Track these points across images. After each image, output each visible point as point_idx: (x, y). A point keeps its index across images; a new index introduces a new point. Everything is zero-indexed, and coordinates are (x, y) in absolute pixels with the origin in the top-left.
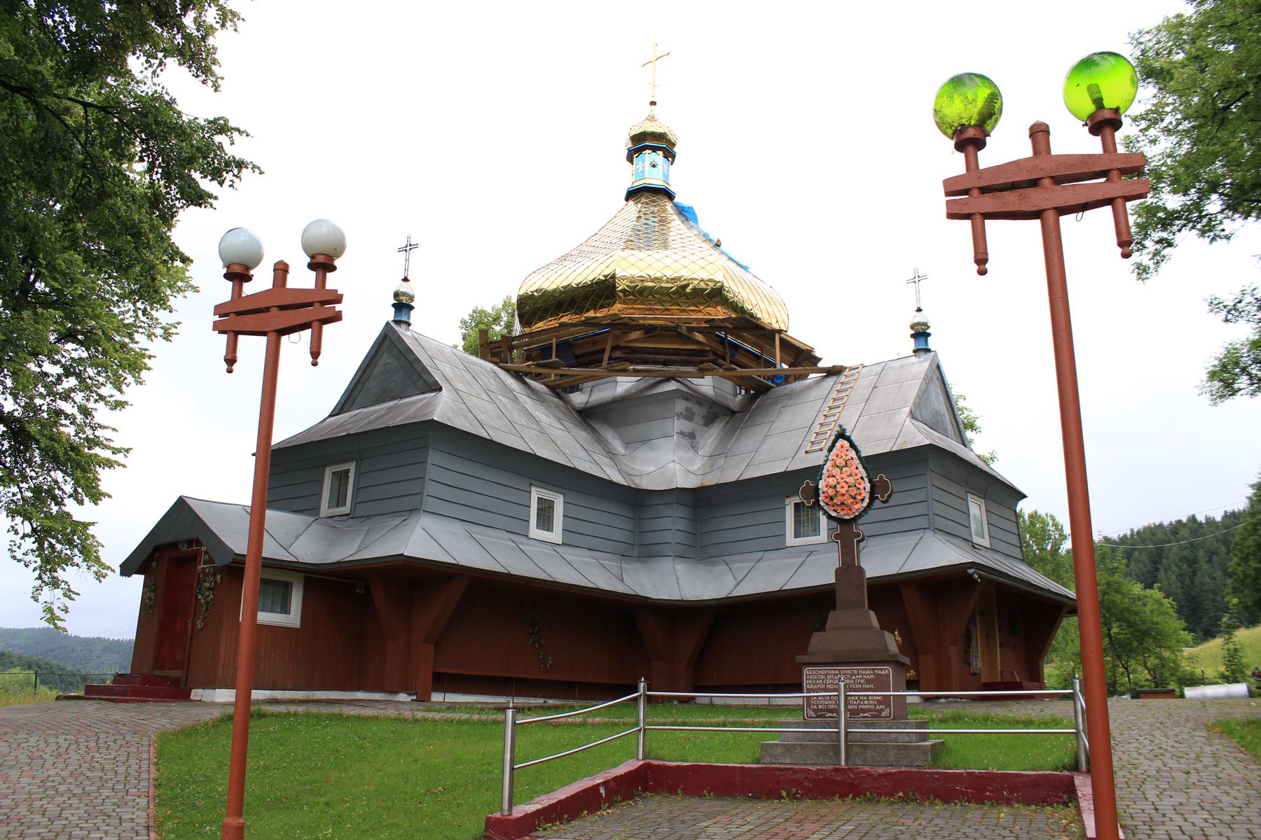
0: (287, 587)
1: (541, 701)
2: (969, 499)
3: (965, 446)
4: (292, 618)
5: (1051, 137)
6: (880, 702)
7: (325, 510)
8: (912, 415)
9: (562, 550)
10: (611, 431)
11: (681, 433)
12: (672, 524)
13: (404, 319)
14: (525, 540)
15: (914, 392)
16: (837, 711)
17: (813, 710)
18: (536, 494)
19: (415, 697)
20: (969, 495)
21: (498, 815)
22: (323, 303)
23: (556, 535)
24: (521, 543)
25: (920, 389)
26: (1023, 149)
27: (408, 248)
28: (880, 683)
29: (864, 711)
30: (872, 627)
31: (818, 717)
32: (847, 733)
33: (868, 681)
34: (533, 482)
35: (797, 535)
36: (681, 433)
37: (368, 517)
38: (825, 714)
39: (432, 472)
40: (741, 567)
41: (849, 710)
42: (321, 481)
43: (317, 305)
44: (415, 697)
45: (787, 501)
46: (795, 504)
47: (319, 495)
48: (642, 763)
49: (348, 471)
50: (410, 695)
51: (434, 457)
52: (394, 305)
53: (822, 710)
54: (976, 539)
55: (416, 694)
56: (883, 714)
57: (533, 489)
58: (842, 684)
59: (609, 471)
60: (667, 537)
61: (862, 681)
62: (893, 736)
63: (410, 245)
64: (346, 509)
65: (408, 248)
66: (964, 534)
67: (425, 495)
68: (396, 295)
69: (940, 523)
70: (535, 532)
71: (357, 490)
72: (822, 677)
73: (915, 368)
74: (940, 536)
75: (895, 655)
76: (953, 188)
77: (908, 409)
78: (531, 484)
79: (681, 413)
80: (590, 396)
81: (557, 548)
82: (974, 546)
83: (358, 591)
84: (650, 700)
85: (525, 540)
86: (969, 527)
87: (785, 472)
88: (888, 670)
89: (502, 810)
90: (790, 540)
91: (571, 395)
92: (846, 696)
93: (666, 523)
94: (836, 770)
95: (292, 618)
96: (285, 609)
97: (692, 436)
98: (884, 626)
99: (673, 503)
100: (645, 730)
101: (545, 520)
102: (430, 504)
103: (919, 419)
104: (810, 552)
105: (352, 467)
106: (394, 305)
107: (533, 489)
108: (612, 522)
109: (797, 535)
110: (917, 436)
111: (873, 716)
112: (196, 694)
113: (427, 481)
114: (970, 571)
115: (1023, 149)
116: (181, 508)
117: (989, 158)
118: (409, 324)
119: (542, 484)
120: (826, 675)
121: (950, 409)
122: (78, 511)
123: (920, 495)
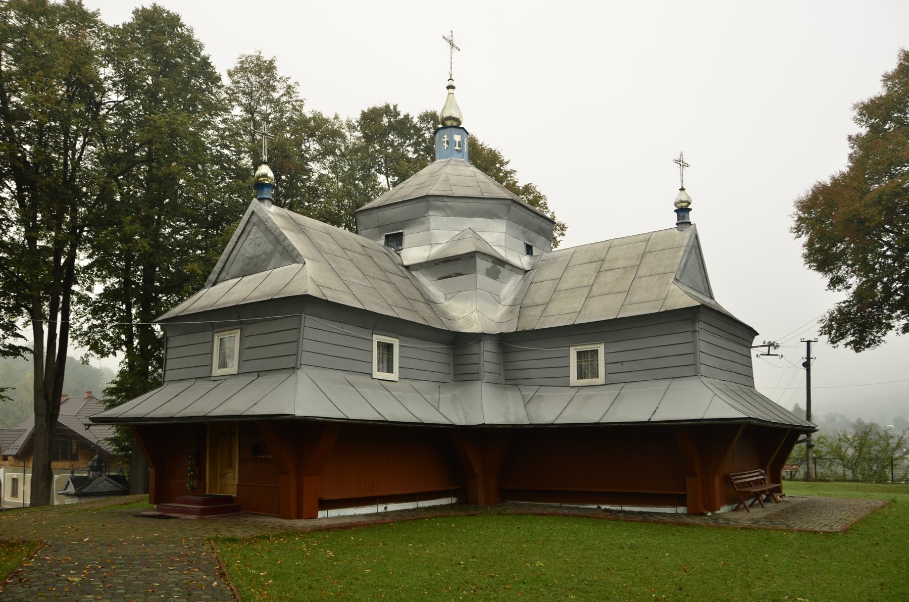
18: (377, 338)
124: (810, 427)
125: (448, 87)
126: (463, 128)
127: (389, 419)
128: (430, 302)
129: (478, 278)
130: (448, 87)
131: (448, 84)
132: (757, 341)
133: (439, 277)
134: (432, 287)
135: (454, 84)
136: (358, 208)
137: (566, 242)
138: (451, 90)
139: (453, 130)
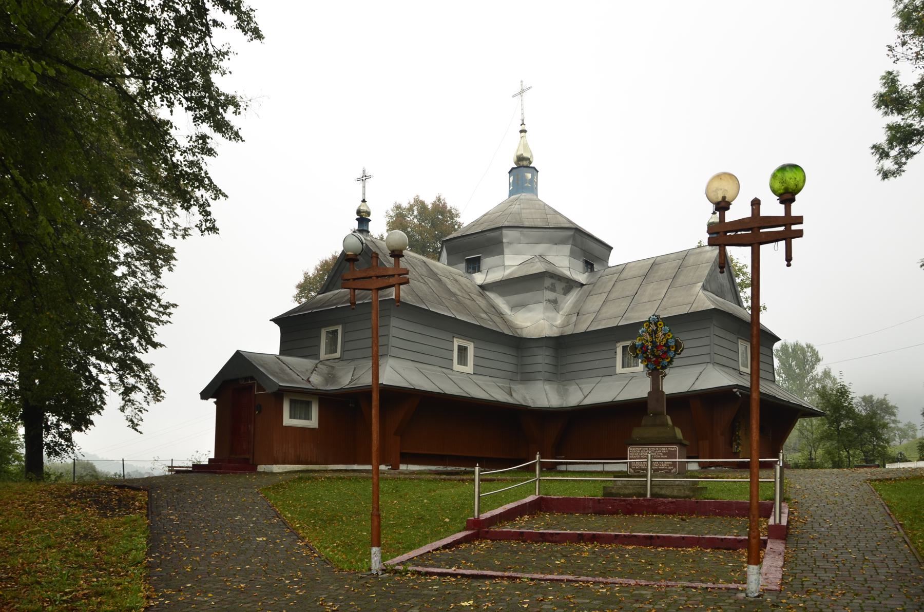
0: (308, 404)
1: (463, 469)
2: (739, 343)
3: (740, 306)
4: (313, 422)
5: (761, 206)
6: (670, 465)
7: (323, 355)
8: (704, 288)
9: (474, 377)
10: (501, 298)
11: (549, 301)
12: (542, 360)
13: (365, 228)
14: (450, 372)
15: (706, 272)
16: (646, 470)
17: (633, 469)
18: (457, 342)
19: (390, 467)
20: (739, 340)
21: (472, 518)
22: (399, 275)
23: (469, 368)
24: (450, 374)
25: (710, 269)
26: (747, 213)
27: (364, 178)
28: (671, 455)
29: (661, 470)
30: (668, 424)
31: (636, 473)
32: (651, 481)
33: (664, 454)
34: (455, 335)
35: (623, 367)
36: (549, 301)
37: (353, 360)
38: (639, 472)
39: (394, 331)
40: (587, 387)
41: (653, 469)
42: (319, 337)
43: (396, 276)
44: (390, 467)
45: (618, 345)
46: (623, 347)
47: (319, 346)
48: (538, 497)
49: (336, 331)
50: (387, 466)
51: (394, 322)
52: (357, 219)
53: (638, 469)
54: (742, 369)
55: (391, 465)
56: (672, 471)
57: (455, 340)
58: (649, 455)
59: (501, 326)
60: (540, 368)
61: (661, 454)
62: (677, 483)
63: (365, 176)
64: (338, 355)
65: (364, 178)
66: (733, 364)
67: (390, 346)
68: (359, 212)
69: (718, 359)
70: (457, 367)
71: (343, 343)
72: (639, 452)
73: (709, 254)
74: (717, 367)
75: (681, 440)
76: (712, 228)
77: (701, 284)
78: (453, 337)
79: (548, 287)
80: (487, 275)
81: (470, 376)
82: (741, 373)
83: (350, 405)
84: (542, 465)
85: (451, 371)
86: (738, 361)
87: (617, 326)
88: (676, 448)
89: (474, 516)
90: (619, 369)
91: (474, 275)
92: (652, 462)
93: (539, 359)
94: (644, 500)
95: (313, 422)
96: (308, 417)
97: (555, 302)
98: (675, 423)
99: (542, 347)
100: (540, 480)
101: (463, 360)
102: (393, 351)
103: (709, 290)
104: (632, 377)
105: (340, 329)
106: (357, 219)
107: (455, 340)
108: (503, 359)
109: (623, 367)
110: (705, 301)
111: (666, 472)
112: (261, 468)
113: (391, 337)
114: (735, 390)
115: (747, 213)
116: (238, 356)
117: (730, 216)
118: (369, 232)
119: (462, 337)
120: (641, 451)
121: (731, 282)
122: (144, 357)
123: (706, 341)
124: (801, 405)
125: (521, 131)
126: (534, 168)
127: (474, 396)
128: (501, 315)
129: (390, 340)
130: (521, 131)
131: (521, 128)
132: (777, 346)
133: (626, 270)
134: (501, 303)
135: (526, 128)
136: (446, 236)
137: (614, 260)
138: (523, 134)
139: (525, 169)
